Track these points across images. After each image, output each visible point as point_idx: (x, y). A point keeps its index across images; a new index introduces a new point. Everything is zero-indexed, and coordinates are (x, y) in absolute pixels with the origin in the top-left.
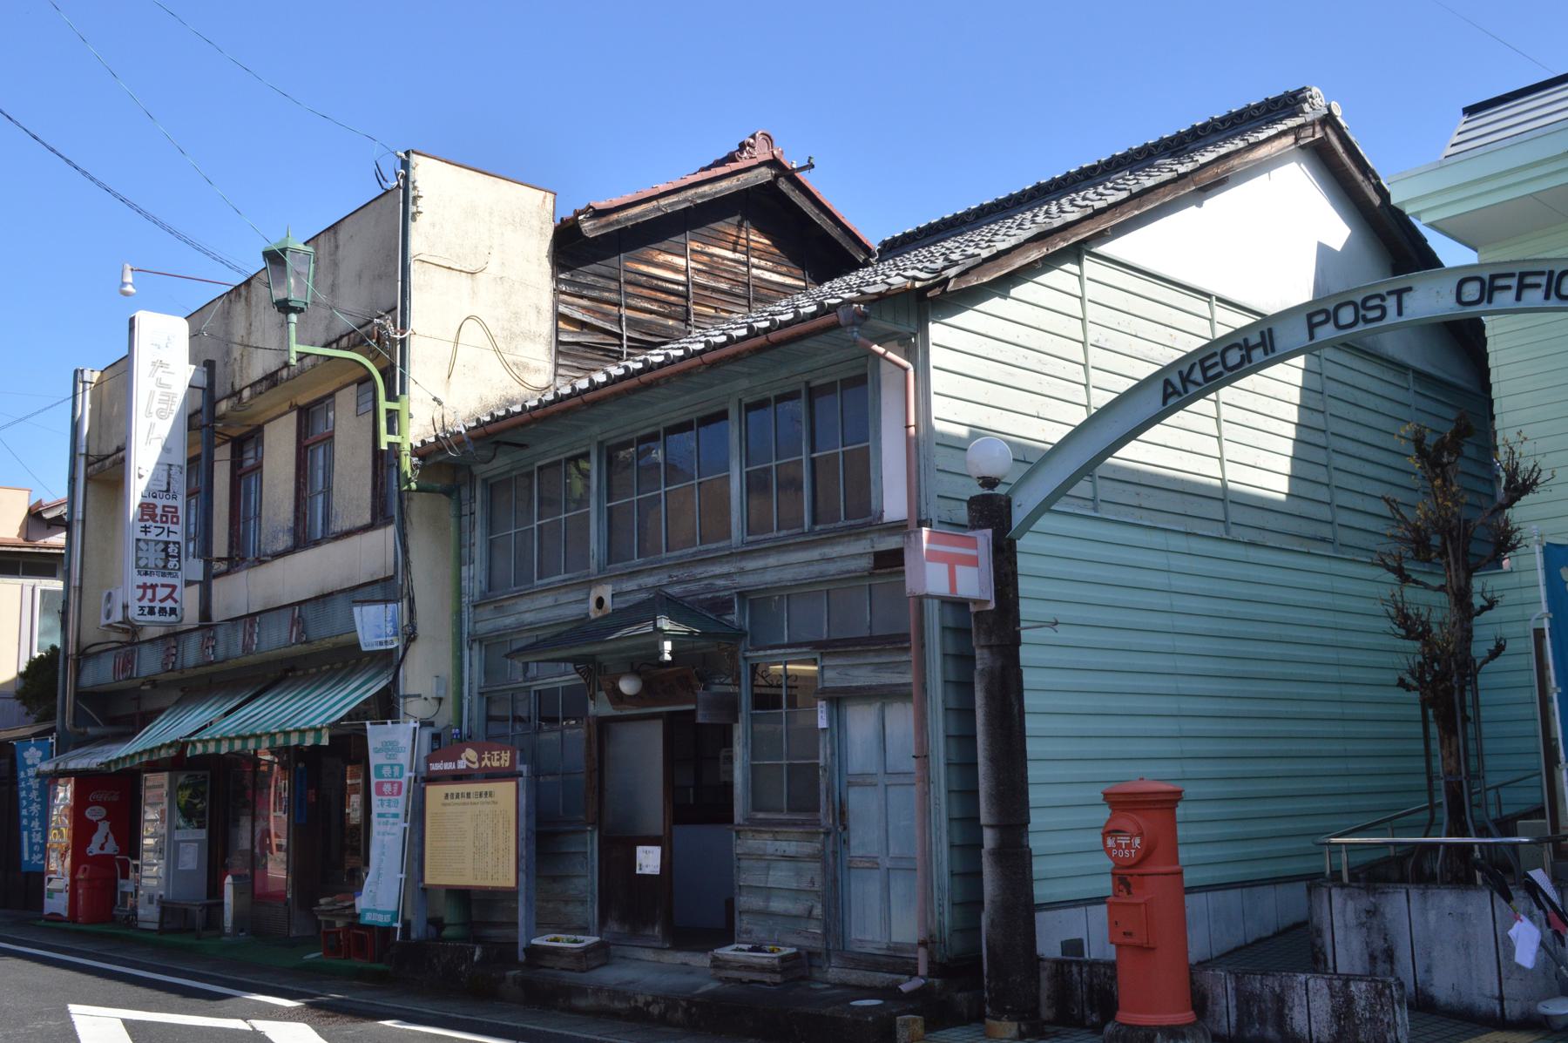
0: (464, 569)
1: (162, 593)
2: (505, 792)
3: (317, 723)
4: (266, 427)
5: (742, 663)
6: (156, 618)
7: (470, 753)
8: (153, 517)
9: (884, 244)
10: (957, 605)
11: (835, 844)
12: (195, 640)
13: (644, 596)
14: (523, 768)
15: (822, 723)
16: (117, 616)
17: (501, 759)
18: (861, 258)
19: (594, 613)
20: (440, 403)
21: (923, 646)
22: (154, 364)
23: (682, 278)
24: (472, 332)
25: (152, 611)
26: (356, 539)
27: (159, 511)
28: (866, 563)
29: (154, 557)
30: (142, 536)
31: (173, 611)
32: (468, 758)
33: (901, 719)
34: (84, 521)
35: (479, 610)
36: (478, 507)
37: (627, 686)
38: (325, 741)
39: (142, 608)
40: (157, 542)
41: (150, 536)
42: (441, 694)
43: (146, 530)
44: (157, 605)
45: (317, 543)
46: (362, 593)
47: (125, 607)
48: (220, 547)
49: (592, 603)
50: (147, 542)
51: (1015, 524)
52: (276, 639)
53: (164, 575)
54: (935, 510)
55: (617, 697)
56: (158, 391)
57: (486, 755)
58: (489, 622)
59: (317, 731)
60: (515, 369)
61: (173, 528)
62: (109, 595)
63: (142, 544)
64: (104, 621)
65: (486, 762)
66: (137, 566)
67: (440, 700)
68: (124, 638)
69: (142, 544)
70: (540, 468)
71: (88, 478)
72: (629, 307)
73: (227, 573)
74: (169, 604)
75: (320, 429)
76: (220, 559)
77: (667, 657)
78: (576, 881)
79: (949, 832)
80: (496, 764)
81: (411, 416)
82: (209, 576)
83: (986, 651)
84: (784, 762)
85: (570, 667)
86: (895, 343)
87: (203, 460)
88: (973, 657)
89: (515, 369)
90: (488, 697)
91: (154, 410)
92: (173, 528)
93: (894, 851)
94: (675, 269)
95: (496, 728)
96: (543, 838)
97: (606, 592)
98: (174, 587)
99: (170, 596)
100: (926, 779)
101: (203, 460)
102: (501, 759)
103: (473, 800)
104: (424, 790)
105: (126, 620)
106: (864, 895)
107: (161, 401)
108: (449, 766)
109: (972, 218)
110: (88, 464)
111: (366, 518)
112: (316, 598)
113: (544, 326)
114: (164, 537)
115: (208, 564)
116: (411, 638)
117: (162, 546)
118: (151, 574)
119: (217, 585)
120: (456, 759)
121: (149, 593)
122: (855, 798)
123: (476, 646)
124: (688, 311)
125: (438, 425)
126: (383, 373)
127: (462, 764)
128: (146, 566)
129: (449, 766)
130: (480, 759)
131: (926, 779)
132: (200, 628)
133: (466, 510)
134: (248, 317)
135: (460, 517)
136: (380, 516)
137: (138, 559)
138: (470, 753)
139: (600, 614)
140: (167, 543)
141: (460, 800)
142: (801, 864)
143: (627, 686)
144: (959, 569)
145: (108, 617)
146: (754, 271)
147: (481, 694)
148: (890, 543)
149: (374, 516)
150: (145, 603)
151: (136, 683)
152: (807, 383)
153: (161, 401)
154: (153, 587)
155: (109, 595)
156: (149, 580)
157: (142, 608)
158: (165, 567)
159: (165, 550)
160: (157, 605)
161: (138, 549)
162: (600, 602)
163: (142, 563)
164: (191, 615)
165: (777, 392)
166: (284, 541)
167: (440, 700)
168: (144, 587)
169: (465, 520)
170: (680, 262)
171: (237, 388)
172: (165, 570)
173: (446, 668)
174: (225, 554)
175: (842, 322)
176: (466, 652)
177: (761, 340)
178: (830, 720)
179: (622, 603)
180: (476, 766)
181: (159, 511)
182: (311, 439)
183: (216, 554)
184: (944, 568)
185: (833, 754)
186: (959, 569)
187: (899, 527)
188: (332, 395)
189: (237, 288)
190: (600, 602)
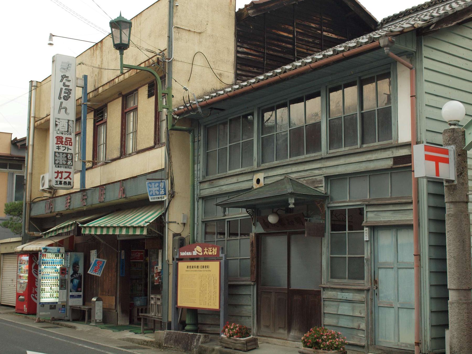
0: (196, 166)
1: (65, 175)
2: (215, 267)
3: (141, 224)
4: (108, 104)
5: (326, 209)
6: (63, 186)
7: (199, 248)
8: (62, 143)
9: (384, 20)
10: (436, 182)
11: (372, 295)
12: (79, 196)
13: (279, 178)
14: (221, 255)
15: (366, 238)
16: (46, 186)
17: (214, 251)
18: (373, 27)
19: (255, 186)
20: (187, 90)
21: (418, 202)
22: (62, 76)
23: (291, 36)
24: (199, 61)
25: (61, 183)
26: (147, 153)
27: (64, 140)
28: (390, 163)
29: (62, 160)
30: (57, 150)
31: (70, 183)
32: (198, 250)
33: (406, 239)
34: (33, 145)
35: (201, 185)
36: (202, 138)
37: (272, 219)
38: (145, 233)
39: (57, 182)
40: (63, 153)
41: (60, 151)
42: (185, 221)
43: (58, 148)
44: (63, 180)
45: (130, 155)
46: (151, 176)
47: (50, 181)
48: (89, 156)
49: (255, 181)
50: (59, 153)
51: (467, 144)
52: (113, 196)
53: (66, 168)
54: (425, 137)
55: (266, 224)
56: (64, 88)
57: (206, 249)
58: (207, 191)
59: (142, 228)
60: (219, 76)
61: (70, 147)
62: (43, 177)
63: (57, 154)
64: (41, 188)
65: (206, 252)
66: (55, 163)
67: (184, 224)
68: (48, 195)
69: (57, 154)
70: (231, 120)
71: (35, 128)
72: (268, 49)
73: (91, 168)
74: (68, 180)
75: (131, 105)
76: (89, 162)
77: (291, 206)
78: (245, 307)
79: (430, 291)
80: (210, 253)
81: (173, 96)
82: (83, 172)
83: (452, 206)
84: (347, 256)
85: (244, 210)
86: (405, 56)
87: (82, 133)
88: (444, 208)
89: (219, 76)
90: (206, 223)
91: (62, 96)
92: (70, 147)
93: (401, 300)
94: (289, 32)
95: (209, 238)
96: (230, 289)
97: (261, 176)
98: (70, 173)
99: (68, 177)
100: (419, 267)
101: (82, 133)
102: (214, 251)
103: (199, 269)
104: (177, 264)
105: (51, 188)
106: (386, 319)
107: (65, 93)
108: (189, 254)
109: (426, 6)
110: (35, 122)
111: (152, 144)
112: (130, 178)
113: (232, 58)
114: (66, 151)
115: (84, 163)
116: (172, 195)
117: (65, 155)
118: (61, 167)
119: (88, 173)
120: (192, 250)
121: (60, 175)
122: (382, 275)
123: (201, 201)
124: (294, 49)
125: (186, 99)
126: (161, 78)
127: (195, 253)
128: (58, 164)
129: (189, 254)
130: (203, 251)
131: (419, 267)
132: (81, 191)
133: (196, 139)
134: (102, 57)
135: (194, 142)
136: (157, 143)
137: (55, 160)
138: (199, 248)
139: (258, 186)
140: (67, 154)
141: (194, 269)
142: (355, 304)
143: (272, 219)
144: (441, 164)
145: (43, 186)
146: (325, 33)
147: (203, 222)
148: (403, 152)
149: (155, 143)
150: (58, 179)
151: (55, 214)
152: (360, 77)
153: (65, 93)
154: (62, 173)
155: (43, 177)
156: (60, 170)
157: (57, 182)
158: (66, 164)
159: (67, 157)
160: (63, 180)
161: (55, 156)
162: (258, 181)
163: (57, 162)
164: (77, 186)
165: (345, 82)
166: (116, 154)
167: (184, 224)
168: (58, 172)
169: (196, 144)
170: (291, 28)
171: (97, 87)
172: (66, 166)
173: (187, 211)
174: (88, 186)
175: (382, 45)
176: (196, 203)
177: (340, 55)
178: (370, 237)
179: (269, 181)
180: (201, 254)
181: (64, 140)
182: (128, 109)
183: (87, 159)
184: (433, 163)
185: (371, 253)
186: (441, 164)
187: (408, 145)
188: (137, 90)
189: (97, 44)
190: (258, 181)
